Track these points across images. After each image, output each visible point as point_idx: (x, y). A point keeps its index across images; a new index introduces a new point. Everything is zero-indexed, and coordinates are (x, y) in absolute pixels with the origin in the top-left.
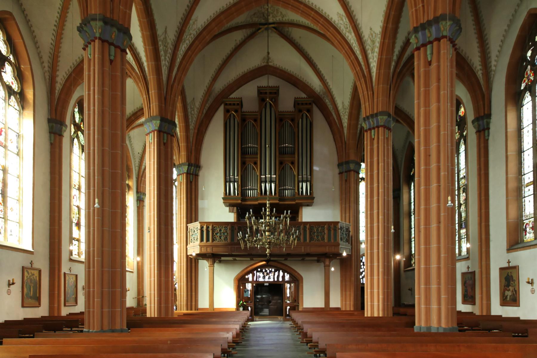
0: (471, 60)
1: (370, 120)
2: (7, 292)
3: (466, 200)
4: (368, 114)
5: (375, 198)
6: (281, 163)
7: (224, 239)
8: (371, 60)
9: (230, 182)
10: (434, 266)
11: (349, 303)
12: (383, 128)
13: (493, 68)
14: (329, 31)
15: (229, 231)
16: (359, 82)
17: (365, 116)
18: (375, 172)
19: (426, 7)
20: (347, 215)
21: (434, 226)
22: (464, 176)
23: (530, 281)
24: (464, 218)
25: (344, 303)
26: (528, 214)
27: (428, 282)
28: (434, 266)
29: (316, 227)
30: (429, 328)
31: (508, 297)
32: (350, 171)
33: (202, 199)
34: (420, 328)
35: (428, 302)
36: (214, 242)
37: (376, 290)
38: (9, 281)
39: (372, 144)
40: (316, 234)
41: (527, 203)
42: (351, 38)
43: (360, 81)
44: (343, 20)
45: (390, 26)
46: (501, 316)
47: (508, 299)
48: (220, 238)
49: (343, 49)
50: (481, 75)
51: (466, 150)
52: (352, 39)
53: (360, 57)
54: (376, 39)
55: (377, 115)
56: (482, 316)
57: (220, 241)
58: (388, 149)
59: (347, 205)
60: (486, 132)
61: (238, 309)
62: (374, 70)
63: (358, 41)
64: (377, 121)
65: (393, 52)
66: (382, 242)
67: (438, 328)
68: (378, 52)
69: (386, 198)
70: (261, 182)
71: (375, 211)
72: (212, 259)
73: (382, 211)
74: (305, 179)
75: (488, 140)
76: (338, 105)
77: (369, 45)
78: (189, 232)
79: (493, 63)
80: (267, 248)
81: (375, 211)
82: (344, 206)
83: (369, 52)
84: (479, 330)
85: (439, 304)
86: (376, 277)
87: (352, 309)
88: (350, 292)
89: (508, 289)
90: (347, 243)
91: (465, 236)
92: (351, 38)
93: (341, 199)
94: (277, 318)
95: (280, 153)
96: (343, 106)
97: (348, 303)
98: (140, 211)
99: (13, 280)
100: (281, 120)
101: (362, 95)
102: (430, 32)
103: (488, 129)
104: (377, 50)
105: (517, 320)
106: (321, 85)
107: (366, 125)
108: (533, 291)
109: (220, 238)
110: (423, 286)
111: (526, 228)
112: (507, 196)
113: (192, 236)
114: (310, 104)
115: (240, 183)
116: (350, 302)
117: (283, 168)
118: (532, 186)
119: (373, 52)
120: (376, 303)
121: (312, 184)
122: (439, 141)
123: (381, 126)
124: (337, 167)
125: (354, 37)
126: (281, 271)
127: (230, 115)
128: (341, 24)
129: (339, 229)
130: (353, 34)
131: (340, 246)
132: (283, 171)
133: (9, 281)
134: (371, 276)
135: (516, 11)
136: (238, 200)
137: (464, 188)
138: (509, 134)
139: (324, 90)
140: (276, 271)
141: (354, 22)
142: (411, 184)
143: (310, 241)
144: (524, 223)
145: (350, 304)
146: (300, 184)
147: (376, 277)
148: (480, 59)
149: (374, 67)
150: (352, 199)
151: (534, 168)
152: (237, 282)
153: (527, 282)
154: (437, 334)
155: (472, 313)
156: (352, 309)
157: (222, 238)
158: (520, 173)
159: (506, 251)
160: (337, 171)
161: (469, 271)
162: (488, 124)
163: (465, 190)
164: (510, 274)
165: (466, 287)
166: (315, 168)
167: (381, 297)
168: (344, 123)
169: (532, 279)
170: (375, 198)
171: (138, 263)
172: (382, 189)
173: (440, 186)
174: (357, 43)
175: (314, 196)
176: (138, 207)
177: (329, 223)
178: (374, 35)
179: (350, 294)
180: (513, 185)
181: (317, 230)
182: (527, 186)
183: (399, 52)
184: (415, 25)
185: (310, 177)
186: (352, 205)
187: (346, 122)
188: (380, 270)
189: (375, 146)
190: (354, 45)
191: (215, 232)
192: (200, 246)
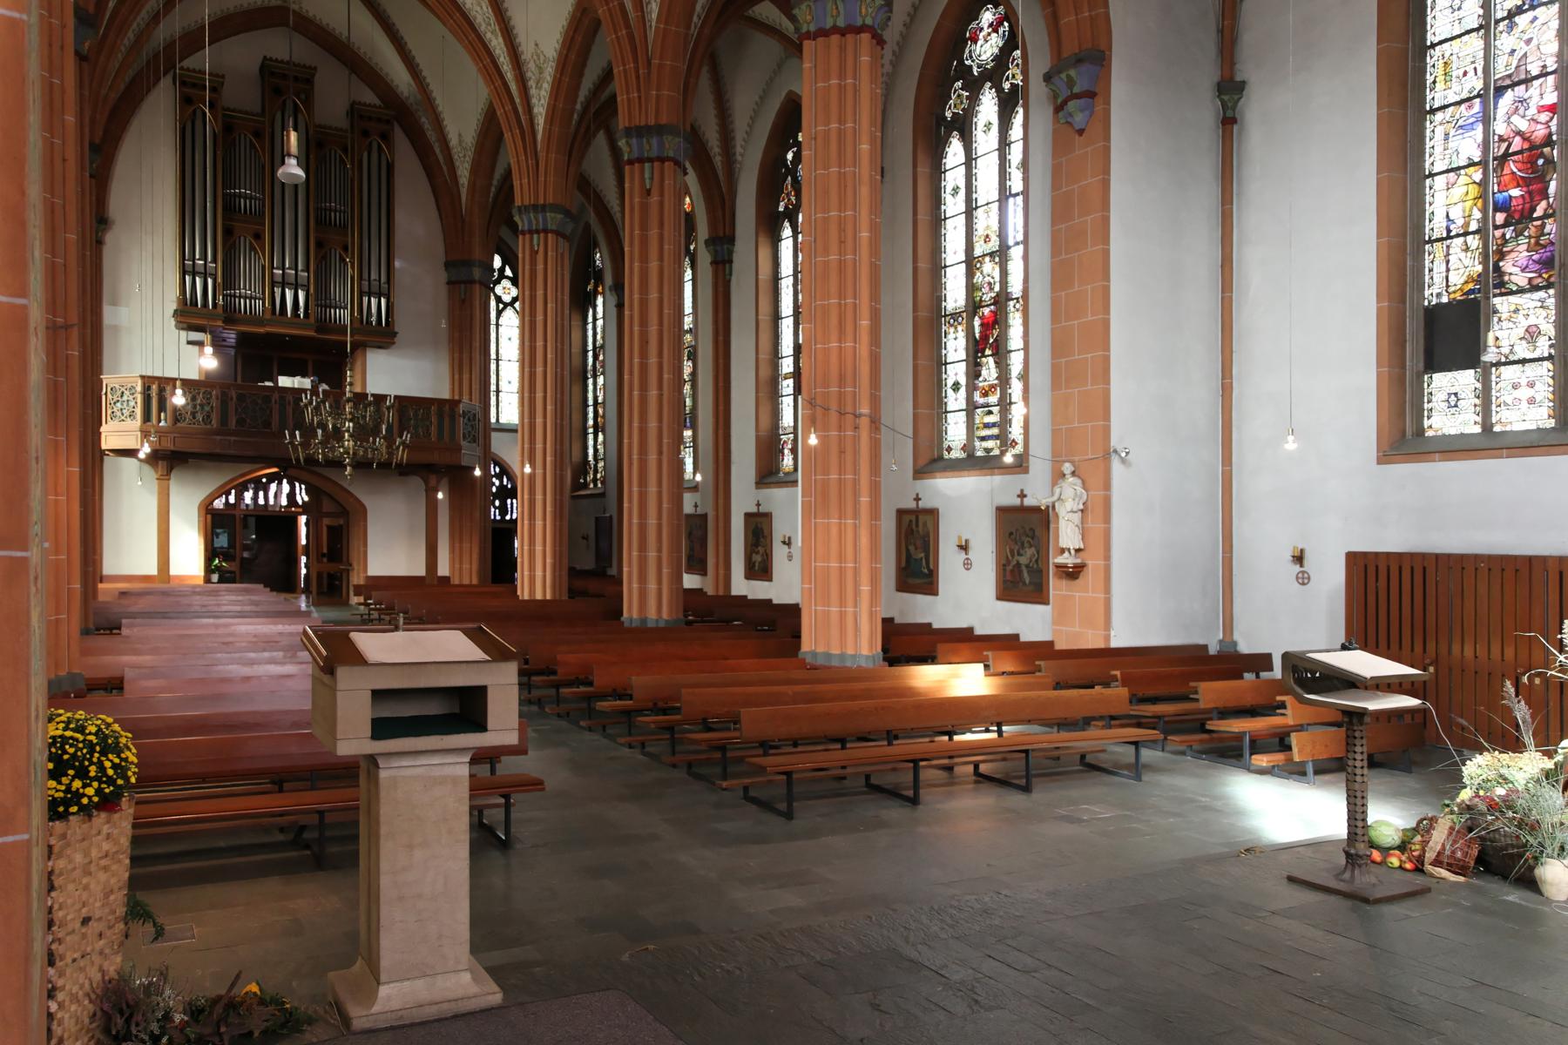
0: (704, 134)
1: (532, 215)
2: (964, 564)
3: (694, 374)
4: (526, 202)
5: (539, 370)
6: (319, 245)
7: (203, 419)
8: (534, 101)
9: (194, 274)
10: (652, 521)
11: (468, 566)
12: (555, 236)
13: (739, 158)
14: (452, 18)
15: (214, 403)
16: (510, 134)
17: (520, 204)
18: (540, 318)
19: (643, 99)
20: (466, 376)
21: (652, 457)
22: (690, 329)
23: (787, 540)
24: (690, 410)
25: (457, 566)
26: (786, 425)
27: (643, 547)
28: (652, 521)
29: (413, 409)
30: (644, 620)
31: (757, 564)
32: (472, 282)
33: (115, 303)
34: (631, 620)
35: (643, 579)
36: (179, 424)
37: (539, 548)
39: (533, 262)
40: (412, 422)
41: (785, 406)
42: (497, 44)
43: (511, 131)
44: (482, 8)
45: (573, 57)
46: (746, 597)
47: (757, 568)
48: (194, 418)
49: (464, 38)
50: (719, 164)
51: (694, 280)
52: (498, 47)
53: (513, 87)
54: (545, 65)
55: (544, 208)
56: (716, 597)
57: (194, 424)
58: (563, 275)
59: (465, 356)
60: (727, 266)
61: (207, 580)
62: (540, 121)
63: (509, 55)
64: (545, 220)
65: (576, 96)
66: (551, 456)
67: (657, 620)
68: (549, 89)
69: (559, 370)
70: (273, 284)
71: (539, 395)
72: (165, 463)
73: (552, 396)
74: (375, 289)
75: (729, 281)
76: (450, 136)
77: (532, 72)
78: (106, 394)
79: (739, 150)
80: (348, 464)
81: (539, 395)
82: (456, 355)
83: (532, 83)
84: (712, 622)
85: (659, 582)
86: (539, 523)
87: (475, 581)
88: (471, 543)
89: (756, 550)
90: (474, 445)
91: (692, 444)
92: (497, 44)
93: (451, 340)
95: (318, 222)
96: (460, 142)
97: (466, 566)
100: (320, 145)
101: (516, 159)
102: (648, 142)
103: (731, 262)
104: (546, 86)
105: (767, 603)
106: (412, 82)
107: (523, 221)
109: (194, 418)
110: (635, 553)
111: (783, 448)
112: (757, 392)
113: (115, 403)
114: (388, 122)
115: (219, 280)
116: (471, 564)
117: (324, 257)
118: (792, 380)
119: (539, 87)
120: (539, 573)
121: (393, 303)
122: (661, 323)
123: (552, 231)
124: (444, 268)
125: (503, 45)
126: (285, 481)
127: (194, 112)
128: (477, 11)
129: (460, 416)
130: (501, 39)
131: (463, 451)
132: (324, 263)
134: (530, 520)
135: (771, 79)
136: (215, 320)
137: (690, 351)
138: (760, 284)
139: (419, 97)
141: (504, 21)
142: (588, 311)
144: (781, 440)
145: (471, 568)
146: (365, 299)
147: (539, 523)
148: (717, 135)
149: (541, 114)
150: (477, 344)
151: (794, 350)
154: (657, 630)
155: (701, 590)
156: (475, 581)
157: (199, 417)
158: (776, 355)
159: (754, 485)
160: (443, 276)
161: (698, 513)
162: (731, 253)
163: (693, 356)
164: (759, 525)
165: (692, 541)
166: (397, 264)
167: (549, 561)
168: (461, 176)
170: (539, 370)
172: (552, 354)
173: (662, 395)
174: (507, 58)
175: (396, 330)
177: (440, 402)
178: (542, 57)
179: (471, 547)
180: (765, 372)
181: (416, 415)
182: (786, 379)
183: (586, 97)
184: (627, 125)
185: (386, 286)
186: (477, 356)
187: (465, 176)
188: (549, 509)
189: (540, 267)
190: (502, 59)
192: (141, 431)
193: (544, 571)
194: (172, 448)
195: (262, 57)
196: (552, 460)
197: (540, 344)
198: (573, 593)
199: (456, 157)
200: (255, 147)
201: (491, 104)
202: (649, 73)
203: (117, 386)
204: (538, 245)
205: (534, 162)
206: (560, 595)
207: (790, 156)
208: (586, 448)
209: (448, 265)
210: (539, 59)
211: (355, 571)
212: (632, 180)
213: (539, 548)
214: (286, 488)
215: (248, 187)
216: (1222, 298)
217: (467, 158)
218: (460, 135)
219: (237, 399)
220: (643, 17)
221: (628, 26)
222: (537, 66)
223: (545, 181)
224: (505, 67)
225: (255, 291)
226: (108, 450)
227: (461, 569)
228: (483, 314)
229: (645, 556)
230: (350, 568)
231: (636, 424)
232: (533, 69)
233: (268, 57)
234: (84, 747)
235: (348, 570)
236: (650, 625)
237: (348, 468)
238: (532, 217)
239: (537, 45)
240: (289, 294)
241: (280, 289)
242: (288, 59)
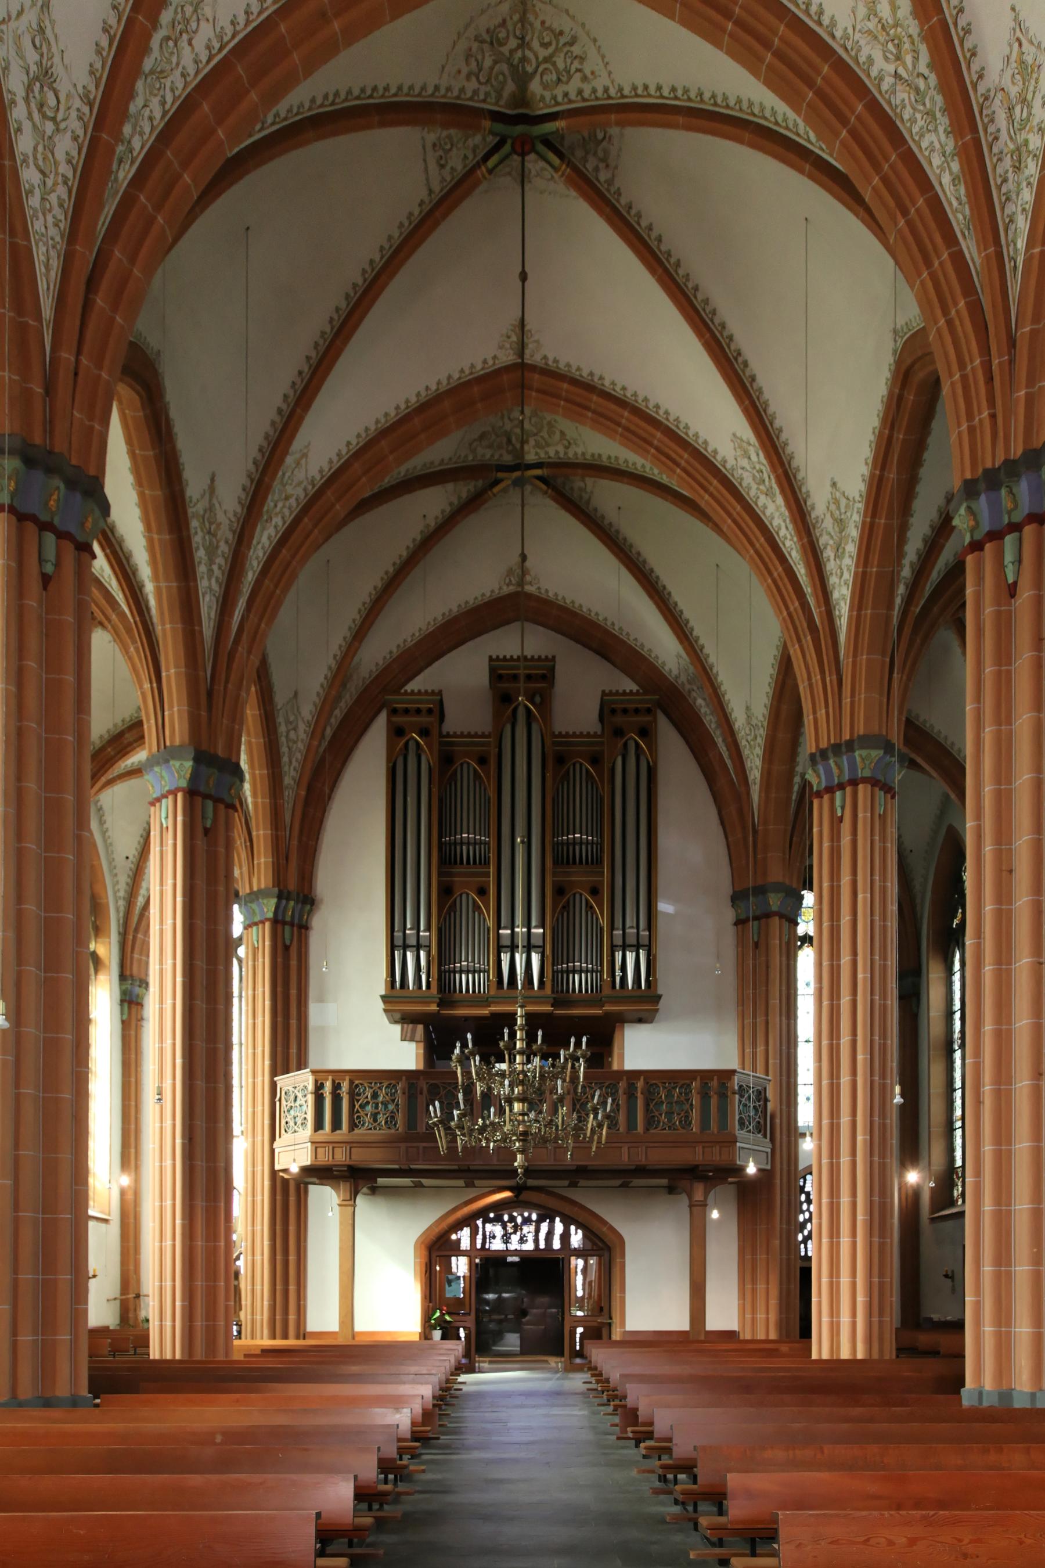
4: (824, 744)
7: (386, 1122)
8: (833, 580)
11: (764, 1316)
14: (706, 490)
15: (400, 1100)
18: (845, 919)
25: (748, 1316)
30: (1006, 1395)
32: (768, 915)
33: (321, 1000)
34: (980, 1394)
36: (356, 1131)
37: (845, 1280)
45: (892, 475)
48: (375, 1120)
52: (777, 514)
53: (801, 571)
54: (849, 514)
55: (850, 746)
57: (375, 1129)
61: (426, 1335)
62: (842, 593)
63: (794, 521)
66: (865, 1134)
67: (1033, 1395)
70: (499, 950)
74: (632, 940)
78: (280, 1100)
80: (518, 1150)
81: (845, 1040)
83: (829, 553)
86: (845, 1240)
87: (773, 1336)
88: (768, 1284)
93: (741, 1002)
94: (546, 1362)
97: (761, 1316)
98: (129, 1035)
100: (561, 760)
104: (851, 548)
107: (819, 776)
109: (375, 1120)
110: (987, 1269)
114: (649, 711)
116: (768, 1313)
120: (845, 1319)
121: (655, 956)
123: (864, 780)
125: (784, 510)
126: (558, 1219)
128: (743, 468)
129: (734, 1093)
130: (780, 500)
131: (738, 1144)
132: (565, 914)
136: (428, 1003)
142: (953, 956)
143: (647, 1129)
145: (768, 1319)
146: (619, 956)
147: (845, 1240)
150: (775, 1002)
152: (425, 1253)
156: (773, 1336)
157: (381, 1118)
160: (729, 915)
166: (664, 907)
167: (860, 1299)
171: (123, 1193)
172: (865, 972)
175: (660, 992)
176: (123, 1022)
178: (843, 502)
179: (768, 1288)
183: (919, 554)
184: (968, 476)
186: (775, 1020)
187: (757, 768)
189: (846, 840)
191: (358, 1101)
192: (312, 1143)
193: (854, 1315)
194: (348, 1162)
195: (487, 659)
196: (865, 1140)
197: (845, 959)
198: (902, 1350)
199: (744, 743)
200: (480, 777)
201: (785, 647)
202: (1011, 362)
203: (291, 1089)
204: (843, 808)
205: (834, 677)
206: (881, 1351)
208: (951, 1150)
209: (737, 898)
210: (839, 508)
212: (980, 579)
213: (845, 1280)
214: (559, 1228)
215: (471, 830)
217: (759, 740)
218: (748, 708)
219: (429, 1091)
220: (999, 255)
221: (968, 287)
222: (835, 520)
223: (852, 703)
224: (788, 543)
225: (473, 961)
227: (753, 1320)
228: (784, 959)
229: (1009, 1274)
231: (988, 1027)
232: (830, 529)
233: (494, 657)
235: (610, 1325)
236: (1018, 1404)
237: (519, 1156)
238: (833, 765)
239: (834, 484)
240: (519, 959)
241: (509, 955)
242: (519, 653)
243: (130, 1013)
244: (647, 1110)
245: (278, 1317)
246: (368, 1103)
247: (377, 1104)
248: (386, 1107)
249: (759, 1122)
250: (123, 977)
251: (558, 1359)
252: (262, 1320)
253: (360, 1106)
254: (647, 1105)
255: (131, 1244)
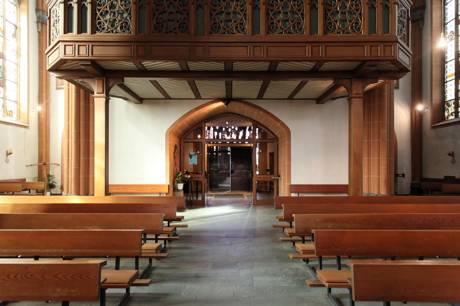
2: (6, 161)
11: (376, 176)
36: (98, 33)
38: (7, 151)
48: (113, 26)
87: (383, 192)
88: (379, 157)
94: (242, 195)
98: (42, 39)
99: (10, 151)
108: (453, 161)
109: (113, 26)
116: (379, 174)
133: (7, 151)
140: (241, 130)
143: (325, 33)
152: (175, 141)
153: (448, 154)
156: (383, 192)
169: (452, 152)
171: (39, 114)
176: (39, 32)
179: (379, 160)
181: (343, 6)
191: (99, 10)
207: (212, 147)
211: (282, 180)
216: (364, 124)
226: (190, 173)
230: (279, 178)
234: (231, 128)
243: (42, 29)
244: (326, 18)
245: (81, 176)
246: (107, 12)
247: (114, 13)
248: (122, 14)
249: (404, 34)
250: (37, 10)
251: (249, 194)
252: (71, 177)
253: (101, 14)
254: (326, 14)
255: (44, 139)
